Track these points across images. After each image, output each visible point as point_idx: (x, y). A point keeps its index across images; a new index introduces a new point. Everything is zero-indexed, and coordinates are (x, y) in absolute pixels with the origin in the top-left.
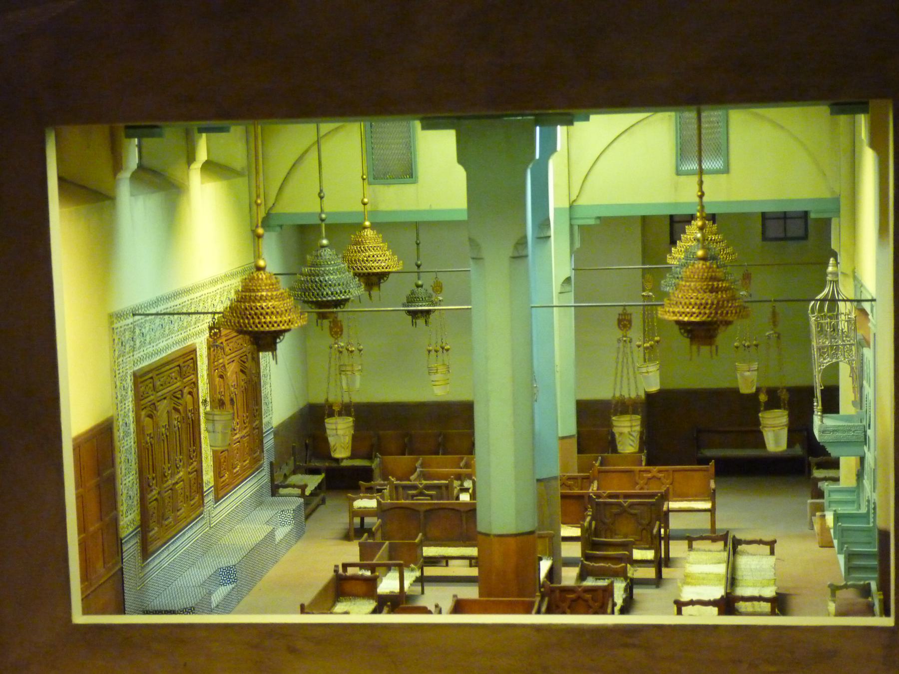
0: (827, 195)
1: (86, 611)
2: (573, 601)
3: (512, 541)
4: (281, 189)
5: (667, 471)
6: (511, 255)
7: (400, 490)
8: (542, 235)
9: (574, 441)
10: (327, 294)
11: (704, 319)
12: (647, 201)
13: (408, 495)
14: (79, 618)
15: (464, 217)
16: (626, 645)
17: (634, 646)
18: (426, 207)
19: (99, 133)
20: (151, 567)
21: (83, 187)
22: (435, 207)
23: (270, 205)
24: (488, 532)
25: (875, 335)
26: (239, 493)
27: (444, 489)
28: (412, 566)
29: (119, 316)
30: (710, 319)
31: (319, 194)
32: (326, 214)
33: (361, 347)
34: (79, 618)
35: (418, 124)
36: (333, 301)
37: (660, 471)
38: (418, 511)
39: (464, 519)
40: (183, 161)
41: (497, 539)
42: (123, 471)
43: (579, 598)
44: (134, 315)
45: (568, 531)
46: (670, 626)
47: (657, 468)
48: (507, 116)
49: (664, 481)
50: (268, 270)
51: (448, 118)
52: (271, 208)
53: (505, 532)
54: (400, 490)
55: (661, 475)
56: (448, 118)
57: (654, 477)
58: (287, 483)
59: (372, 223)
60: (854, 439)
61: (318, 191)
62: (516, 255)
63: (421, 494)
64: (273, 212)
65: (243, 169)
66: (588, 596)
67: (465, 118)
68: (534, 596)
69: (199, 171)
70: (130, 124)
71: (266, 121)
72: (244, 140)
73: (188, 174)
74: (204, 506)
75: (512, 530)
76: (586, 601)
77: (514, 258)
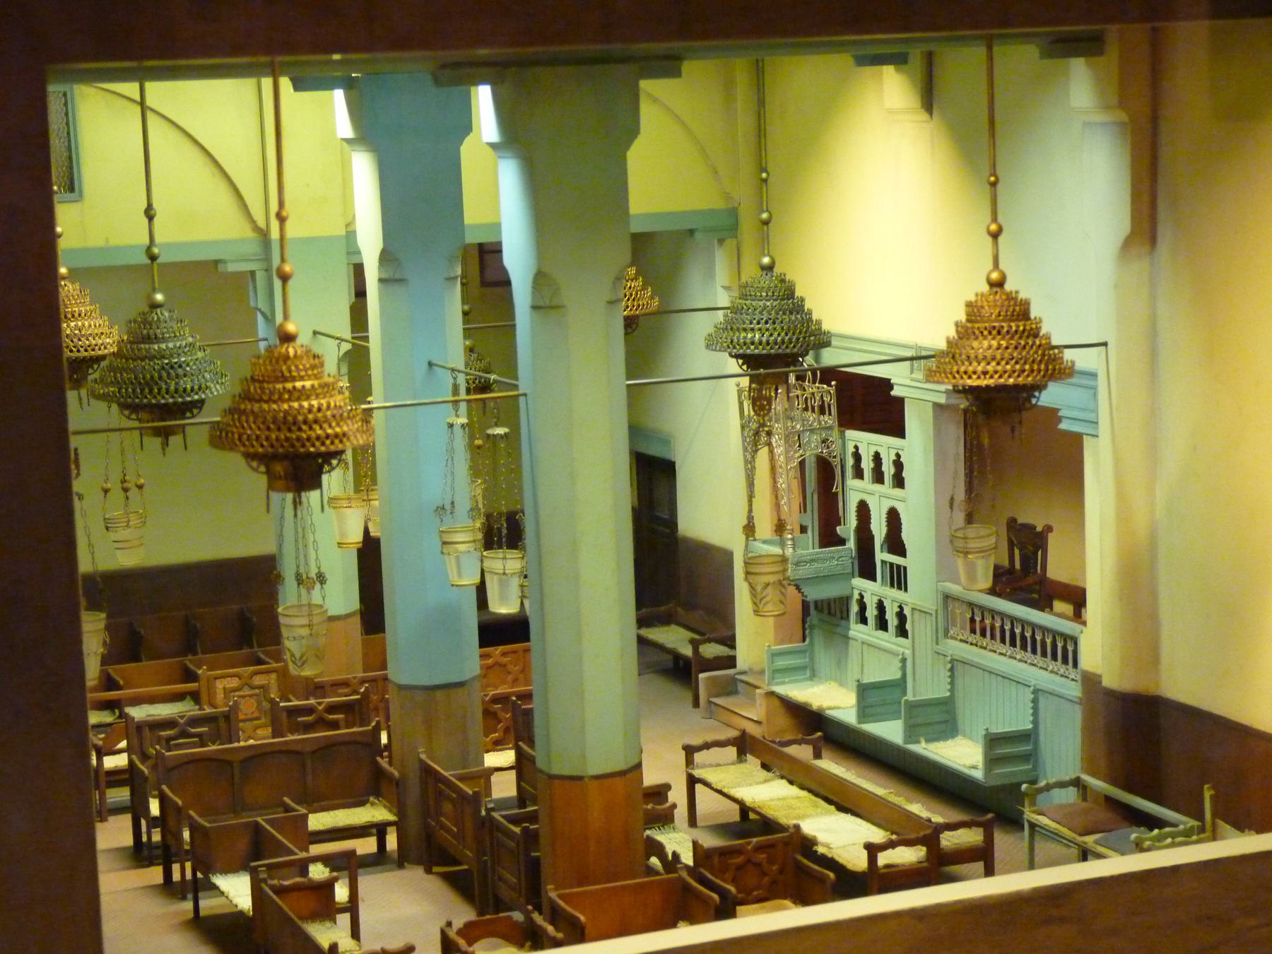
0: (719, 204)
2: (739, 868)
5: (514, 652)
7: (146, 731)
9: (356, 622)
10: (185, 390)
12: (682, 209)
13: (160, 738)
16: (1048, 921)
17: (1062, 920)
18: (101, 243)
21: (1155, 119)
22: (114, 242)
24: (579, 774)
25: (76, 450)
27: (222, 721)
32: (160, 246)
33: (142, 481)
35: (285, 83)
37: (504, 654)
38: (230, 763)
41: (596, 783)
43: (749, 861)
45: (493, 759)
46: (1112, 878)
47: (501, 648)
49: (510, 667)
50: (299, 341)
53: (608, 770)
54: (146, 731)
55: (505, 660)
57: (496, 664)
59: (70, 270)
60: (838, 570)
61: (145, 205)
63: (184, 734)
66: (762, 857)
67: (536, 62)
76: (759, 865)
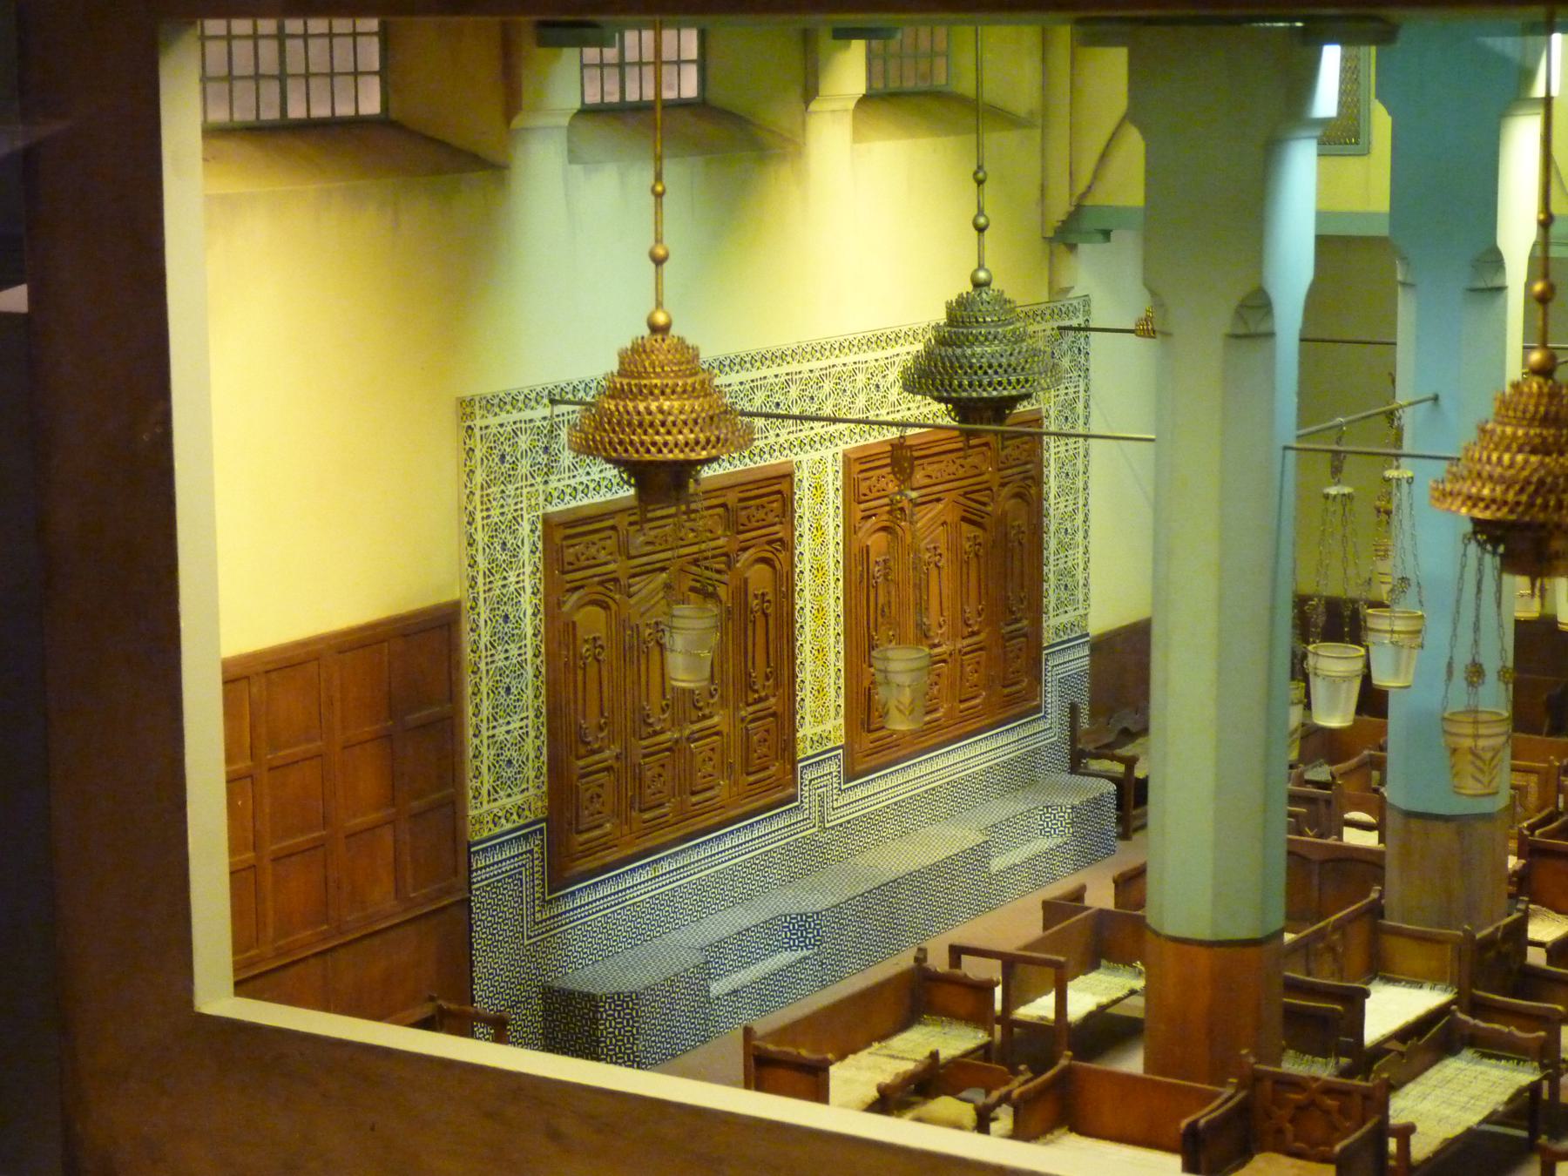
1: (244, 986)
2: (1300, 1108)
3: (1203, 956)
4: (1104, 157)
6: (1227, 329)
8: (1481, 285)
11: (1499, 515)
14: (216, 995)
15: (1383, 230)
19: (475, 36)
20: (578, 903)
21: (441, 144)
23: (1081, 187)
26: (940, 763)
28: (1138, 964)
29: (494, 404)
30: (1513, 517)
31: (975, 174)
34: (216, 995)
36: (992, 399)
39: (1315, 881)
40: (795, 94)
41: (1171, 944)
42: (486, 710)
43: (1312, 1103)
44: (553, 402)
48: (1264, 19)
51: (1121, 20)
52: (1084, 195)
56: (1121, 20)
58: (1118, 752)
62: (1241, 330)
64: (1088, 202)
65: (1031, 113)
66: (1330, 1103)
68: (1223, 1083)
69: (847, 120)
70: (549, 18)
71: (985, 17)
72: (1037, 56)
73: (804, 124)
74: (794, 782)
75: (1205, 934)
76: (1327, 1112)
77: (1237, 337)
